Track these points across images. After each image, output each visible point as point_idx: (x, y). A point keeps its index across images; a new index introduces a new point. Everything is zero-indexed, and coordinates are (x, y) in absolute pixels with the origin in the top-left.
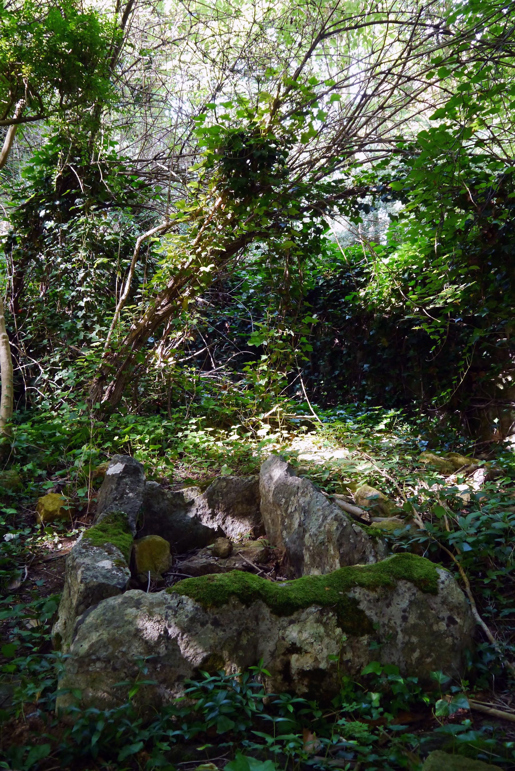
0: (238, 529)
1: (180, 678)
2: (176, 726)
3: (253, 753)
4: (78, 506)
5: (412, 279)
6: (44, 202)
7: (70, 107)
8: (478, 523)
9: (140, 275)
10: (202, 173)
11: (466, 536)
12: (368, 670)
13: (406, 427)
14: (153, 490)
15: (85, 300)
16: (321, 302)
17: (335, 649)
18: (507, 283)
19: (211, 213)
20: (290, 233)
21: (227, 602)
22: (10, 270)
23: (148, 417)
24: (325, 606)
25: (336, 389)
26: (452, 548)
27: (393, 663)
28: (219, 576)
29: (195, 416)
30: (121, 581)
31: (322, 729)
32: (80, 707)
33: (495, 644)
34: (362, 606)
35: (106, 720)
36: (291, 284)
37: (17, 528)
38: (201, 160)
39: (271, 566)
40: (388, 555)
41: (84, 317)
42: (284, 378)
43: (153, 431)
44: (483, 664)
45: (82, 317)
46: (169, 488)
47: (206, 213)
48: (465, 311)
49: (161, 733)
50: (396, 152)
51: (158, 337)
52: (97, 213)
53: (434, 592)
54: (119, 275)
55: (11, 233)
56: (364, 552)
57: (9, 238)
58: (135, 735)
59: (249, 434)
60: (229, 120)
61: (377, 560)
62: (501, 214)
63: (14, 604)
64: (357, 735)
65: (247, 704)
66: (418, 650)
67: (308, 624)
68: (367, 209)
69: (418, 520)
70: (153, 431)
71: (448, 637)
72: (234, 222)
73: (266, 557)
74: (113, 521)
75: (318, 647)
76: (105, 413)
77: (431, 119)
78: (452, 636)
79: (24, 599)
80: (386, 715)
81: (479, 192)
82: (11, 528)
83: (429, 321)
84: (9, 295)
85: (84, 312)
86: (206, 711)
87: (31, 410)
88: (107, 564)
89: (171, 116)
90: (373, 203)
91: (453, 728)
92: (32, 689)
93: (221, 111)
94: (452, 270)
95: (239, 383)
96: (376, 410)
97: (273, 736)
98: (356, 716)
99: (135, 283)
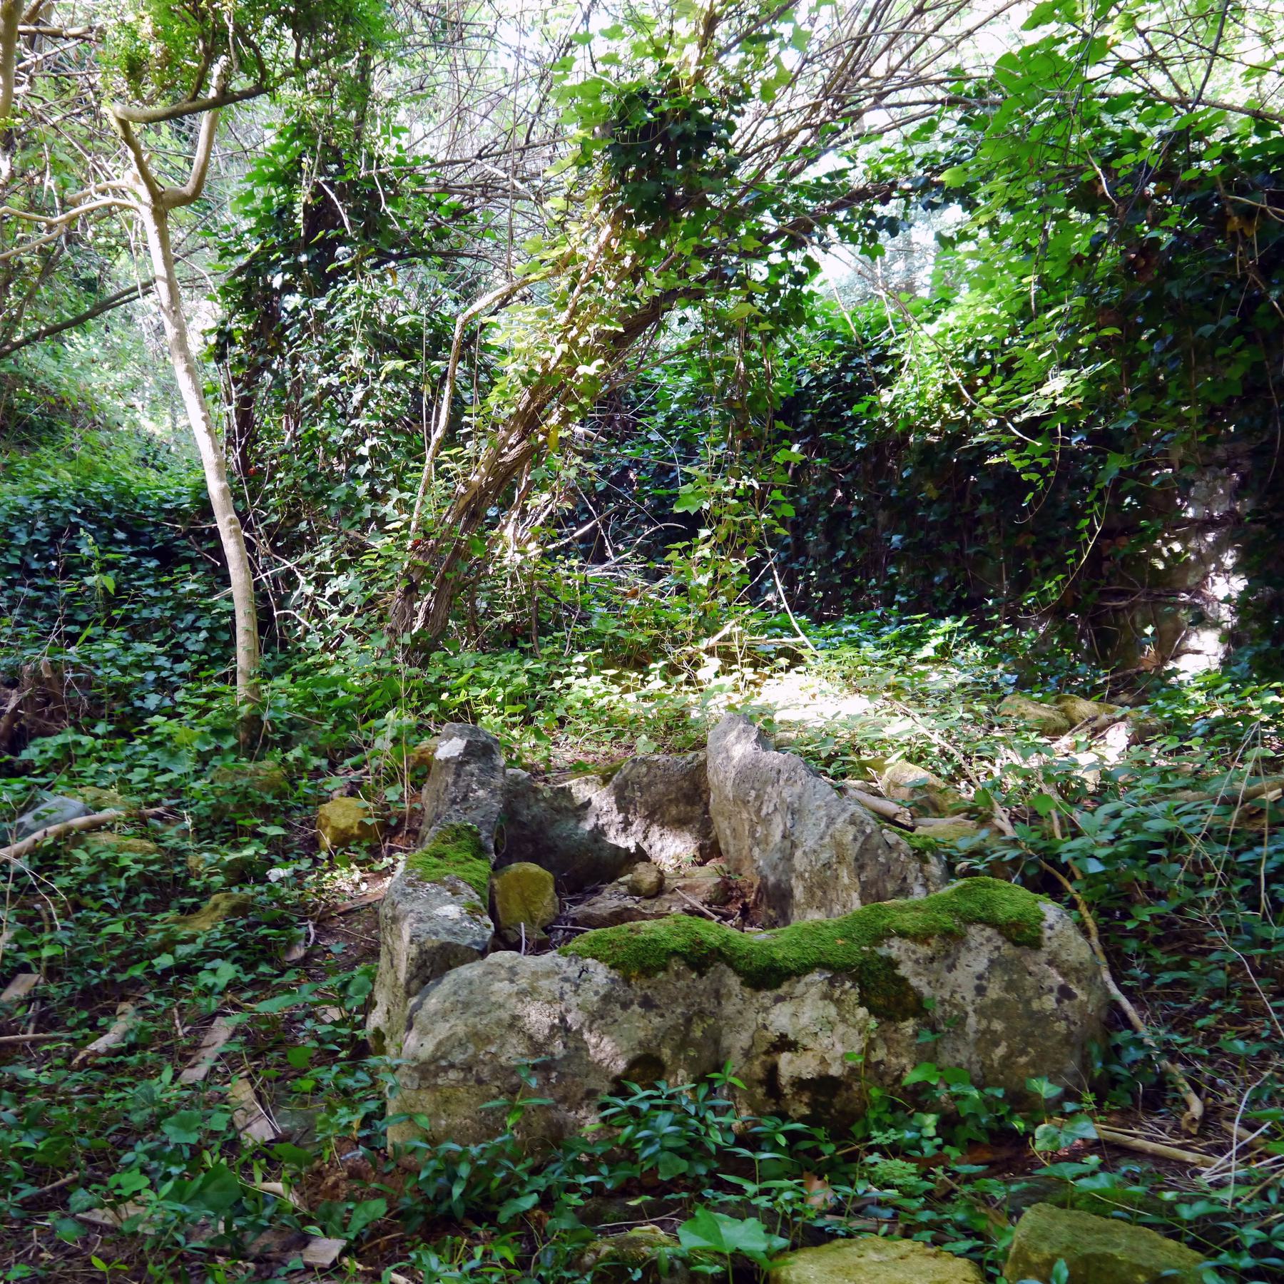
0: (672, 849)
1: (591, 1094)
2: (590, 1168)
3: (723, 1207)
4: (389, 817)
5: (990, 365)
6: (279, 260)
7: (315, 63)
8: (1116, 823)
9: (465, 389)
10: (572, 179)
11: (1092, 847)
12: (911, 1077)
13: (976, 651)
14: (518, 784)
15: (368, 443)
16: (808, 418)
17: (859, 1044)
18: (1175, 358)
19: (591, 257)
20: (745, 287)
21: (665, 968)
22: (228, 395)
23: (498, 654)
24: (837, 971)
25: (841, 586)
26: (1065, 869)
27: (959, 1065)
28: (647, 925)
29: (581, 649)
30: (478, 939)
31: (838, 1172)
32: (428, 1141)
33: (1144, 1032)
34: (903, 971)
35: (472, 1161)
36: (748, 388)
37: (287, 859)
38: (568, 151)
39: (735, 908)
40: (946, 882)
41: (370, 475)
42: (742, 571)
43: (509, 680)
44: (1122, 1066)
45: (366, 476)
46: (546, 780)
47: (583, 259)
48: (1091, 420)
49: (565, 1179)
50: (952, 102)
51: (506, 505)
52: (377, 272)
53: (1036, 944)
54: (427, 390)
55: (224, 323)
56: (905, 879)
57: (221, 333)
58: (522, 1184)
59: (683, 677)
60: (619, 64)
61: (928, 892)
62: (1166, 216)
63: (298, 983)
64: (898, 1181)
65: (707, 1134)
66: (1004, 1044)
67: (809, 1001)
68: (892, 226)
69: (1002, 819)
70: (509, 680)
71: (1058, 1020)
72: (636, 274)
73: (725, 897)
74: (454, 840)
75: (826, 1041)
76: (421, 651)
77: (1025, 27)
78: (1067, 1018)
79: (313, 976)
80: (947, 1149)
81: (1122, 173)
82: (277, 859)
83: (1020, 446)
84: (230, 442)
85: (368, 466)
86: (639, 1145)
87: (288, 653)
88: (452, 911)
89: (499, 66)
90: (905, 214)
91: (1068, 1170)
92: (344, 1115)
93: (600, 47)
94: (1065, 338)
95: (661, 583)
96: (917, 621)
97: (754, 1181)
98: (893, 1151)
99: (458, 405)
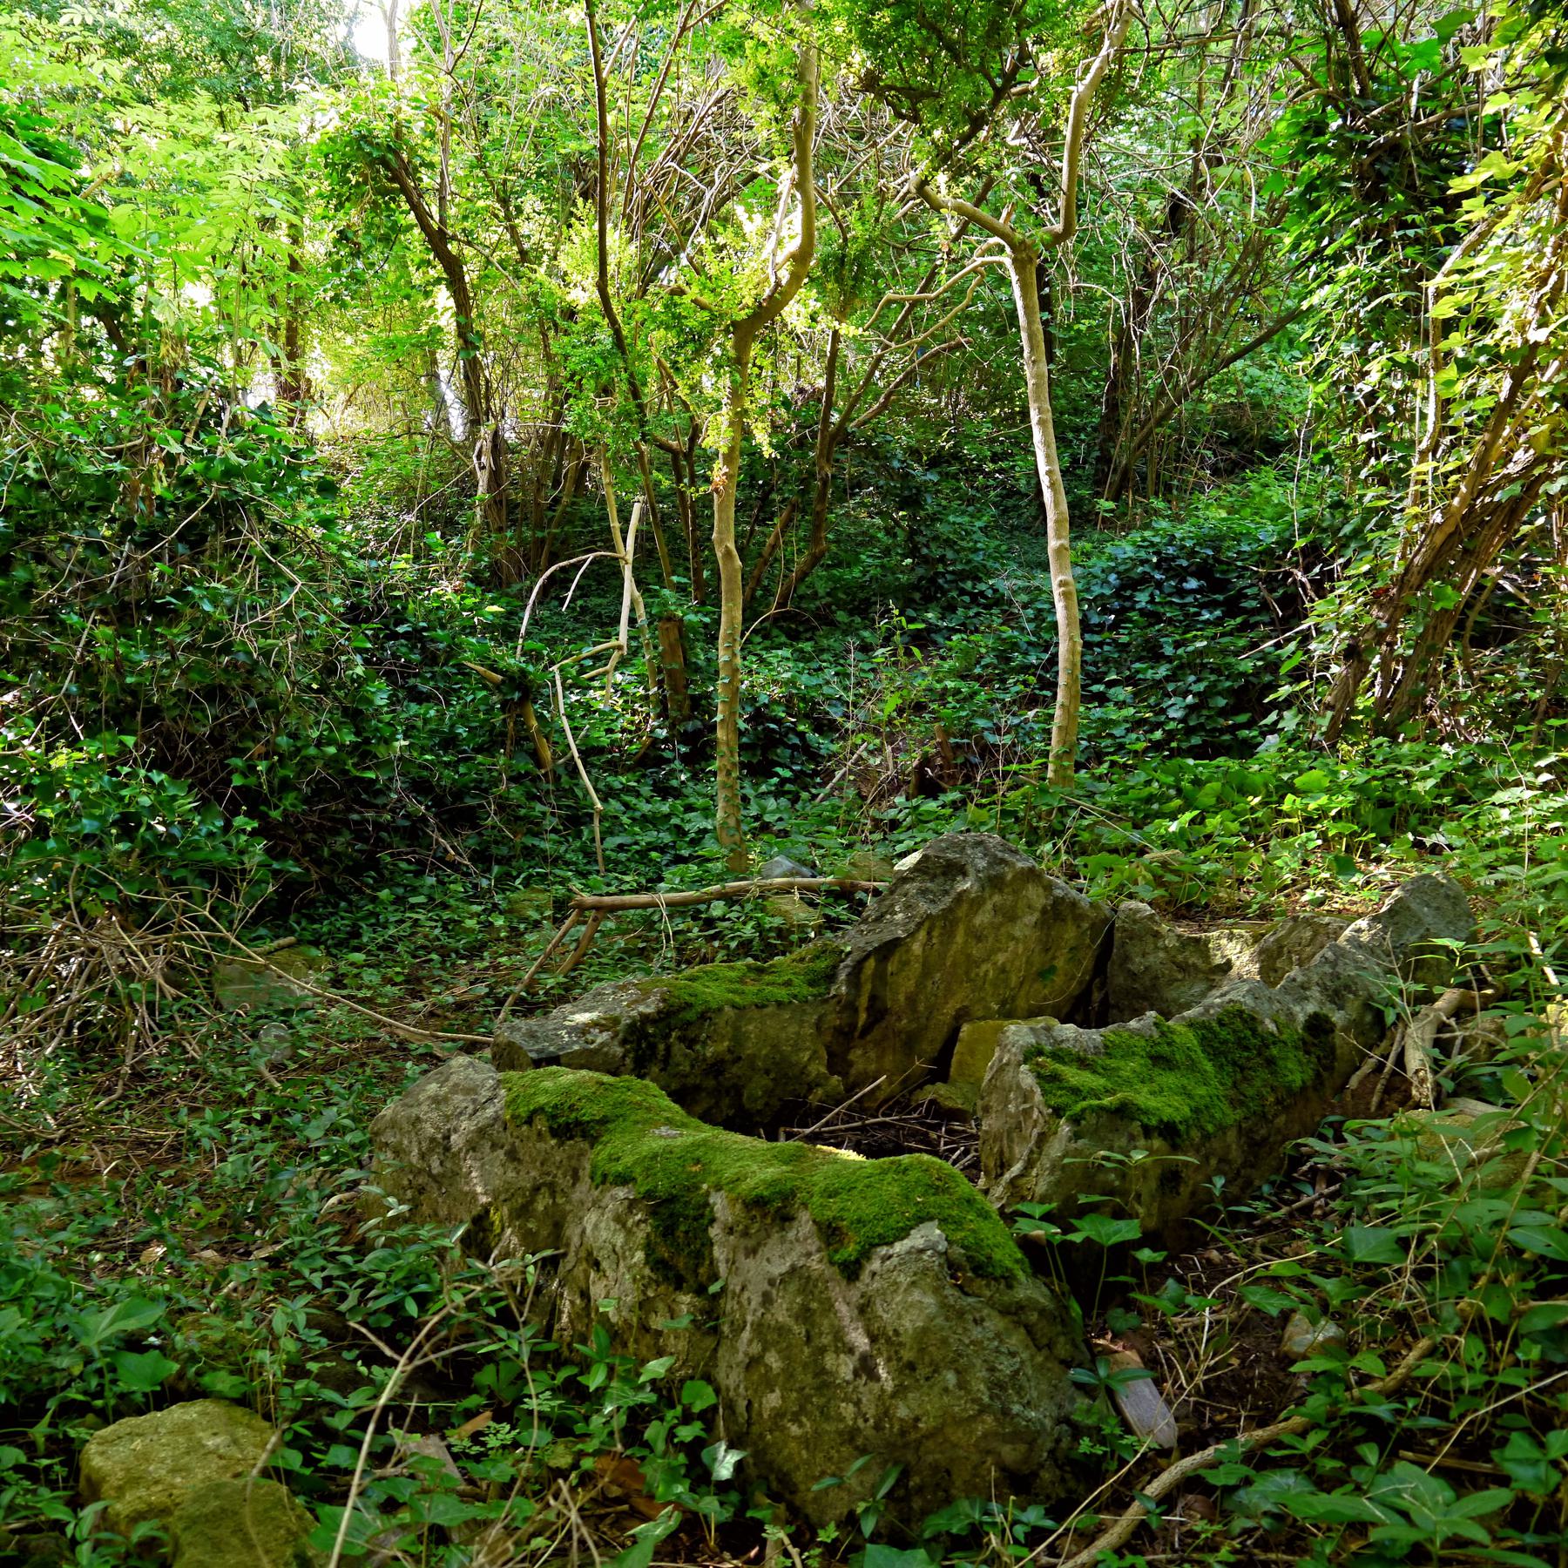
71: (846, 1399)
78: (857, 1403)
